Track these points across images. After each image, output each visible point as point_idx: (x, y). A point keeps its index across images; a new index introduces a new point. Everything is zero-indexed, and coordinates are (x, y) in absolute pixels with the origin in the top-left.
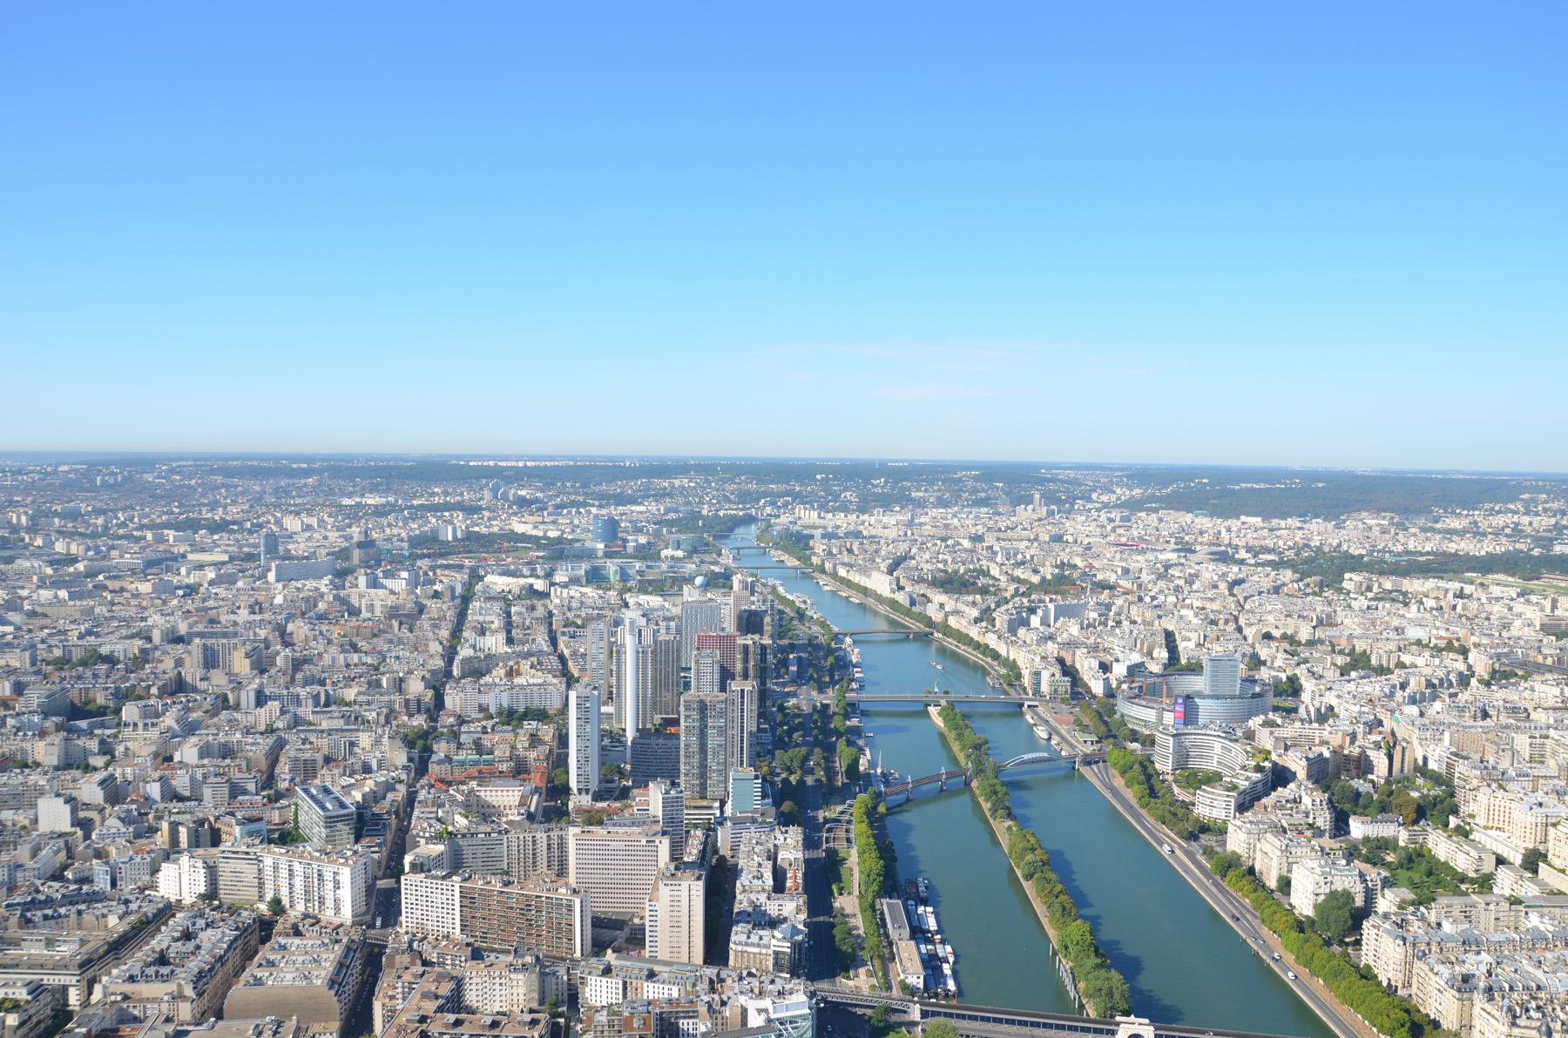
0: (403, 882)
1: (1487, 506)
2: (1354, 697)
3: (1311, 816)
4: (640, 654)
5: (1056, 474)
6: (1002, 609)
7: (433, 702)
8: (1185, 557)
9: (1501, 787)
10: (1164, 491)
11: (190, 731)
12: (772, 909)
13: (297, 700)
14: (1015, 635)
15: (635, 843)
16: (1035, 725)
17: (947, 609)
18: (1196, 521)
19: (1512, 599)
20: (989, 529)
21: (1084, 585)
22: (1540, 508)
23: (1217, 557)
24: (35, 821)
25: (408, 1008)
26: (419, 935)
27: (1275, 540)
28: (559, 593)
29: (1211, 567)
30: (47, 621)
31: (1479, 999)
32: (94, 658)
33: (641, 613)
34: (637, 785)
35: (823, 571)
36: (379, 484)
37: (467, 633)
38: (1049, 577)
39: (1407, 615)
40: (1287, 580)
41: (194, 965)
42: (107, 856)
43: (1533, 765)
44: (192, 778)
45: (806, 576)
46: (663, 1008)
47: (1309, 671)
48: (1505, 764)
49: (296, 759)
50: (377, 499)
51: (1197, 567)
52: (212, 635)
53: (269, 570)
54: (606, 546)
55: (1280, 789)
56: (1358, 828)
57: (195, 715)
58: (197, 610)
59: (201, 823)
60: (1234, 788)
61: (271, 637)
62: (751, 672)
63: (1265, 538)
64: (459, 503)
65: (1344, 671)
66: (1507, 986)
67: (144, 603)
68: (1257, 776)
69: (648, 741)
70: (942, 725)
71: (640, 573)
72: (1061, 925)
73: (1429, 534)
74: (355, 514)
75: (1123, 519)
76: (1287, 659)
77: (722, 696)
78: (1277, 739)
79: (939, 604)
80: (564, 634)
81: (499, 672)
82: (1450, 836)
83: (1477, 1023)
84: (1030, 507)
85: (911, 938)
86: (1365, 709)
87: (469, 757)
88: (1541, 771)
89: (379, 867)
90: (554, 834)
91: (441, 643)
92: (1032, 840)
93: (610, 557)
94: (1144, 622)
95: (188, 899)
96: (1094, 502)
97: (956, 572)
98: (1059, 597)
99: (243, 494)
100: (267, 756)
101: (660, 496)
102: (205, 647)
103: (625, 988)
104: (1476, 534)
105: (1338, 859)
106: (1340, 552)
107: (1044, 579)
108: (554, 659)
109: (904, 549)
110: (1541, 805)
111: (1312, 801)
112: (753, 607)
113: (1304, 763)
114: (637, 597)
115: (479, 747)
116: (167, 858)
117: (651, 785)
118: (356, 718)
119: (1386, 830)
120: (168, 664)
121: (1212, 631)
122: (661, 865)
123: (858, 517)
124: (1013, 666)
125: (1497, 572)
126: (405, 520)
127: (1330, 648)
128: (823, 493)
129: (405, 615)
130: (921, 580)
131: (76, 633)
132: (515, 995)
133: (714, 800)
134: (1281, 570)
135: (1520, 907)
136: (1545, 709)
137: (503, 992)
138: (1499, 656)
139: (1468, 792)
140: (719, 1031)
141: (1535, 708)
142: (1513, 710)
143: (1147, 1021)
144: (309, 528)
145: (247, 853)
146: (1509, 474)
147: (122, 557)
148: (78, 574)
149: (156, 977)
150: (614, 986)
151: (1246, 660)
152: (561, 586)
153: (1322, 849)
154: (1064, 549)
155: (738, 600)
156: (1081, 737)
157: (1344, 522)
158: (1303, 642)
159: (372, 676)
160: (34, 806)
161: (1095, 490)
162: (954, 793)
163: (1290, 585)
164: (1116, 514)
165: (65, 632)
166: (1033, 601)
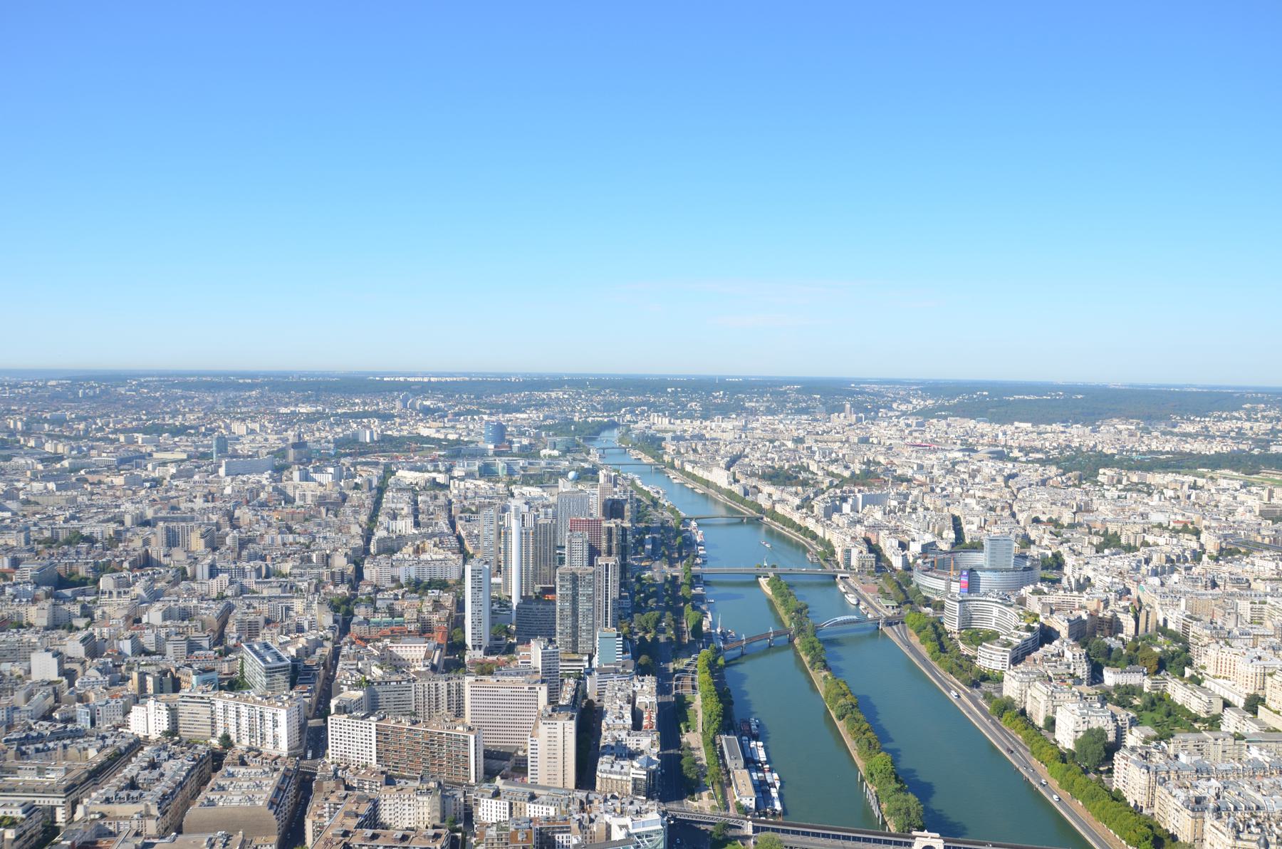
0: (329, 721)
1: (1216, 414)
2: (1107, 570)
3: (1072, 667)
4: (523, 535)
5: (863, 388)
6: (820, 498)
7: (354, 574)
8: (969, 455)
9: (1227, 643)
10: (952, 402)
11: (155, 598)
12: (631, 743)
13: (243, 573)
15: (520, 690)
16: (846, 593)
17: (774, 498)
18: (978, 426)
19: (1236, 490)
20: (809, 433)
21: (886, 479)
22: (1259, 416)
23: (995, 456)
24: (29, 672)
25: (334, 825)
27: (1043, 442)
28: (457, 485)
29: (990, 464)
31: (1209, 817)
32: (77, 538)
33: (524, 501)
34: (521, 642)
35: (673, 467)
36: (310, 396)
37: (382, 518)
38: (858, 472)
39: (1151, 503)
40: (1052, 474)
43: (1254, 626)
45: (659, 471)
46: (542, 824)
47: (1070, 549)
48: (1230, 625)
50: (309, 408)
51: (979, 464)
52: (173, 519)
53: (220, 466)
54: (495, 447)
55: (1046, 645)
56: (1111, 678)
57: (159, 585)
58: (161, 499)
59: (164, 673)
60: (1009, 644)
62: (614, 550)
63: (1034, 440)
64: (375, 411)
65: (1099, 549)
66: (1232, 807)
68: (1028, 635)
69: (530, 606)
70: (770, 593)
72: (868, 757)
73: (1168, 437)
74: (290, 420)
76: (1052, 539)
77: (591, 569)
78: (1044, 604)
79: (767, 494)
80: (461, 518)
81: (408, 550)
82: (1185, 684)
83: (1207, 836)
84: (842, 415)
85: (745, 767)
86: (1116, 580)
87: (384, 619)
88: (1260, 631)
89: (310, 709)
90: (453, 682)
91: (361, 526)
92: (844, 687)
93: (499, 456)
94: (935, 508)
95: (154, 736)
96: (894, 410)
97: (782, 468)
98: (866, 489)
100: (218, 618)
101: (539, 405)
102: (168, 529)
104: (1206, 437)
105: (1094, 702)
106: (1095, 451)
107: (853, 474)
108: (453, 539)
109: (739, 449)
110: (1260, 658)
111: (1073, 656)
112: (616, 497)
113: (1066, 624)
114: (521, 488)
115: (391, 611)
117: (532, 642)
118: (291, 588)
121: (991, 516)
122: (541, 707)
123: (701, 423)
124: (828, 545)
125: (1224, 468)
126: (331, 425)
127: (1087, 530)
128: (672, 404)
130: (753, 475)
131: (62, 518)
132: (421, 813)
133: (584, 654)
134: (1047, 466)
136: (1263, 580)
137: (411, 812)
138: (1225, 537)
139: (1200, 648)
140: (588, 843)
141: (1255, 579)
142: (1237, 581)
143: (937, 835)
144: (252, 432)
146: (1234, 388)
147: (99, 455)
148: (64, 470)
149: (128, 799)
150: (502, 806)
151: (1019, 540)
152: (459, 480)
153: (1081, 695)
154: (870, 449)
155: (603, 491)
156: (884, 603)
157: (1099, 427)
158: (1066, 525)
159: (304, 553)
161: (895, 401)
162: (780, 649)
163: (1055, 479)
164: (912, 421)
165: (53, 517)
166: (845, 492)
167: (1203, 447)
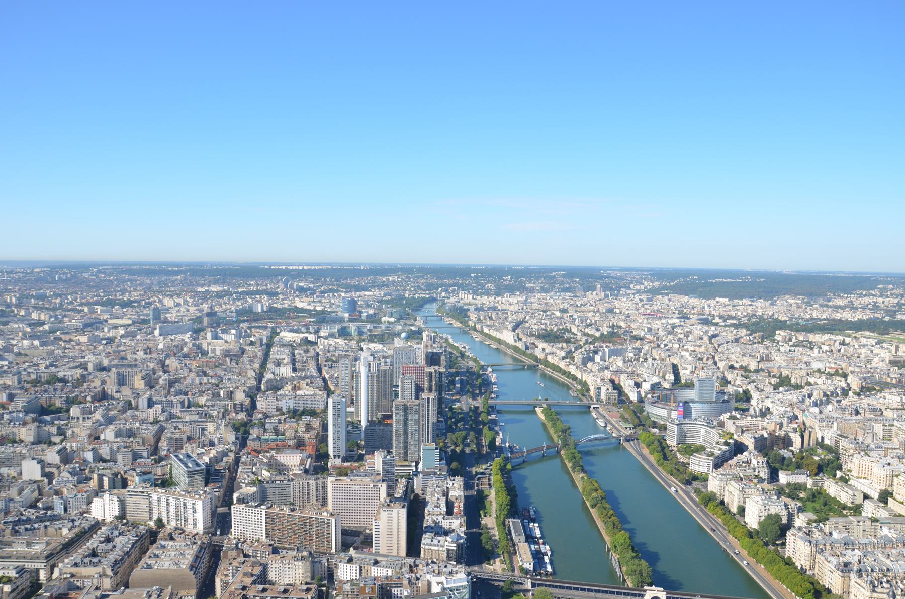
0: (232, 509)
1: (859, 292)
2: (782, 402)
3: (757, 471)
4: (370, 377)
5: (610, 274)
6: (579, 351)
7: (250, 405)
8: (684, 321)
9: (866, 454)
10: (672, 284)
11: (110, 422)
12: (446, 524)
13: (171, 404)
14: (586, 367)
15: (367, 487)
16: (597, 418)
17: (547, 351)
18: (690, 301)
19: (873, 346)
20: (571, 305)
21: (626, 338)
22: (889, 293)
23: (703, 321)
25: (236, 582)
26: (242, 540)
27: (736, 312)
28: (322, 342)
29: (699, 327)
30: (27, 359)
31: (853, 577)
32: (54, 380)
33: (370, 353)
34: (368, 453)
35: (475, 329)
36: (219, 279)
37: (269, 366)
38: (605, 333)
39: (812, 355)
40: (743, 335)
41: (112, 557)
42: (62, 494)
43: (885, 442)
44: (111, 449)
45: (465, 333)
46: (382, 581)
47: (755, 387)
48: (868, 441)
49: (171, 438)
50: (218, 288)
51: (691, 327)
52: (122, 366)
53: (155, 329)
54: (350, 315)
55: (739, 455)
56: (784, 478)
57: (112, 413)
58: (114, 352)
59: (116, 475)
60: (712, 454)
61: (156, 368)
62: (434, 388)
63: (730, 311)
65: (776, 387)
66: (870, 569)
67: (83, 348)
68: (725, 448)
69: (374, 428)
70: (544, 418)
71: (369, 330)
72: (613, 534)
73: (825, 308)
74: (205, 297)
75: (648, 300)
76: (743, 380)
77: (417, 402)
78: (737, 426)
79: (542, 349)
80: (325, 366)
81: (288, 388)
82: (837, 483)
83: (852, 590)
84: (595, 293)
85: (526, 541)
86: (788, 409)
87: (271, 437)
88: (890, 445)
89: (219, 500)
90: (320, 482)
91: (255, 371)
92: (596, 485)
95: (109, 519)
96: (631, 289)
97: (552, 330)
98: (611, 345)
99: (140, 285)
100: (154, 436)
101: (381, 286)
102: (118, 373)
103: (361, 570)
104: (852, 308)
105: (772, 496)
106: (773, 318)
107: (602, 334)
108: (320, 380)
109: (522, 317)
110: (889, 464)
111: (757, 462)
112: (435, 350)
113: (753, 440)
115: (276, 431)
116: (96, 495)
117: (376, 453)
118: (206, 415)
119: (800, 479)
120: (97, 383)
121: (699, 364)
122: (382, 499)
123: (495, 298)
124: (585, 384)
125: (864, 330)
126: (234, 300)
127: (767, 374)
128: (475, 285)
129: (234, 355)
130: (532, 335)
131: (44, 365)
132: (297, 574)
133: (412, 461)
134: (739, 329)
135: (877, 524)
136: (892, 409)
137: (290, 573)
138: (865, 379)
139: (847, 457)
140: (415, 595)
141: (886, 409)
142: (874, 410)
143: (662, 589)
144: (178, 304)
145: (143, 492)
146: (871, 274)
148: (45, 331)
149: (90, 564)
150: (354, 569)
151: (719, 381)
152: (324, 338)
153: (763, 490)
154: (614, 317)
155: (426, 346)
156: (624, 425)
157: (776, 301)
158: (752, 370)
159: (214, 390)
160: (19, 465)
161: (632, 283)
163: (745, 338)
164: (644, 297)
165: (37, 365)
166: (596, 347)
167: (849, 315)
